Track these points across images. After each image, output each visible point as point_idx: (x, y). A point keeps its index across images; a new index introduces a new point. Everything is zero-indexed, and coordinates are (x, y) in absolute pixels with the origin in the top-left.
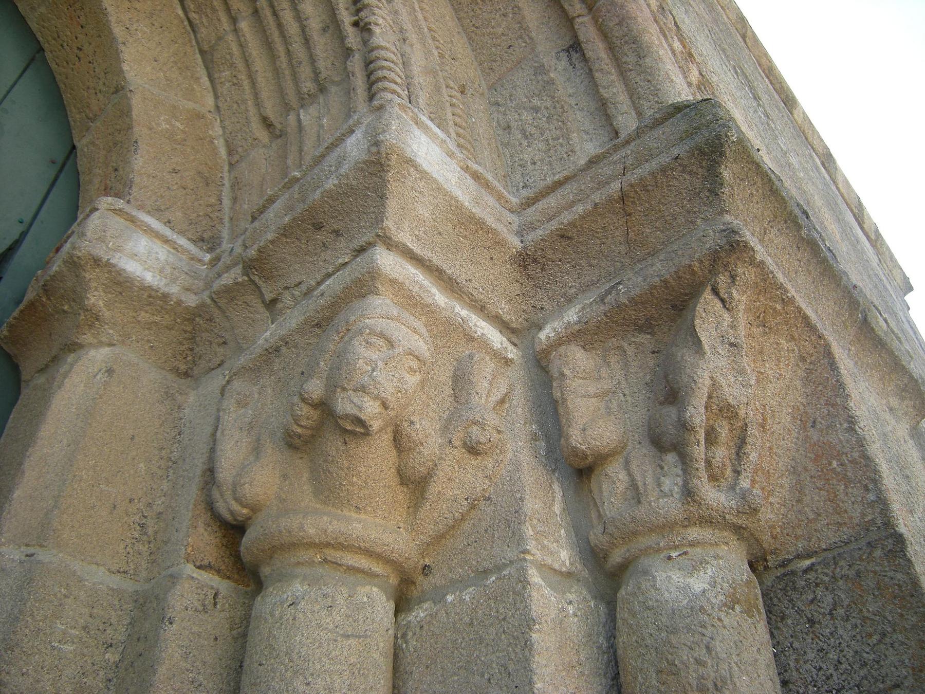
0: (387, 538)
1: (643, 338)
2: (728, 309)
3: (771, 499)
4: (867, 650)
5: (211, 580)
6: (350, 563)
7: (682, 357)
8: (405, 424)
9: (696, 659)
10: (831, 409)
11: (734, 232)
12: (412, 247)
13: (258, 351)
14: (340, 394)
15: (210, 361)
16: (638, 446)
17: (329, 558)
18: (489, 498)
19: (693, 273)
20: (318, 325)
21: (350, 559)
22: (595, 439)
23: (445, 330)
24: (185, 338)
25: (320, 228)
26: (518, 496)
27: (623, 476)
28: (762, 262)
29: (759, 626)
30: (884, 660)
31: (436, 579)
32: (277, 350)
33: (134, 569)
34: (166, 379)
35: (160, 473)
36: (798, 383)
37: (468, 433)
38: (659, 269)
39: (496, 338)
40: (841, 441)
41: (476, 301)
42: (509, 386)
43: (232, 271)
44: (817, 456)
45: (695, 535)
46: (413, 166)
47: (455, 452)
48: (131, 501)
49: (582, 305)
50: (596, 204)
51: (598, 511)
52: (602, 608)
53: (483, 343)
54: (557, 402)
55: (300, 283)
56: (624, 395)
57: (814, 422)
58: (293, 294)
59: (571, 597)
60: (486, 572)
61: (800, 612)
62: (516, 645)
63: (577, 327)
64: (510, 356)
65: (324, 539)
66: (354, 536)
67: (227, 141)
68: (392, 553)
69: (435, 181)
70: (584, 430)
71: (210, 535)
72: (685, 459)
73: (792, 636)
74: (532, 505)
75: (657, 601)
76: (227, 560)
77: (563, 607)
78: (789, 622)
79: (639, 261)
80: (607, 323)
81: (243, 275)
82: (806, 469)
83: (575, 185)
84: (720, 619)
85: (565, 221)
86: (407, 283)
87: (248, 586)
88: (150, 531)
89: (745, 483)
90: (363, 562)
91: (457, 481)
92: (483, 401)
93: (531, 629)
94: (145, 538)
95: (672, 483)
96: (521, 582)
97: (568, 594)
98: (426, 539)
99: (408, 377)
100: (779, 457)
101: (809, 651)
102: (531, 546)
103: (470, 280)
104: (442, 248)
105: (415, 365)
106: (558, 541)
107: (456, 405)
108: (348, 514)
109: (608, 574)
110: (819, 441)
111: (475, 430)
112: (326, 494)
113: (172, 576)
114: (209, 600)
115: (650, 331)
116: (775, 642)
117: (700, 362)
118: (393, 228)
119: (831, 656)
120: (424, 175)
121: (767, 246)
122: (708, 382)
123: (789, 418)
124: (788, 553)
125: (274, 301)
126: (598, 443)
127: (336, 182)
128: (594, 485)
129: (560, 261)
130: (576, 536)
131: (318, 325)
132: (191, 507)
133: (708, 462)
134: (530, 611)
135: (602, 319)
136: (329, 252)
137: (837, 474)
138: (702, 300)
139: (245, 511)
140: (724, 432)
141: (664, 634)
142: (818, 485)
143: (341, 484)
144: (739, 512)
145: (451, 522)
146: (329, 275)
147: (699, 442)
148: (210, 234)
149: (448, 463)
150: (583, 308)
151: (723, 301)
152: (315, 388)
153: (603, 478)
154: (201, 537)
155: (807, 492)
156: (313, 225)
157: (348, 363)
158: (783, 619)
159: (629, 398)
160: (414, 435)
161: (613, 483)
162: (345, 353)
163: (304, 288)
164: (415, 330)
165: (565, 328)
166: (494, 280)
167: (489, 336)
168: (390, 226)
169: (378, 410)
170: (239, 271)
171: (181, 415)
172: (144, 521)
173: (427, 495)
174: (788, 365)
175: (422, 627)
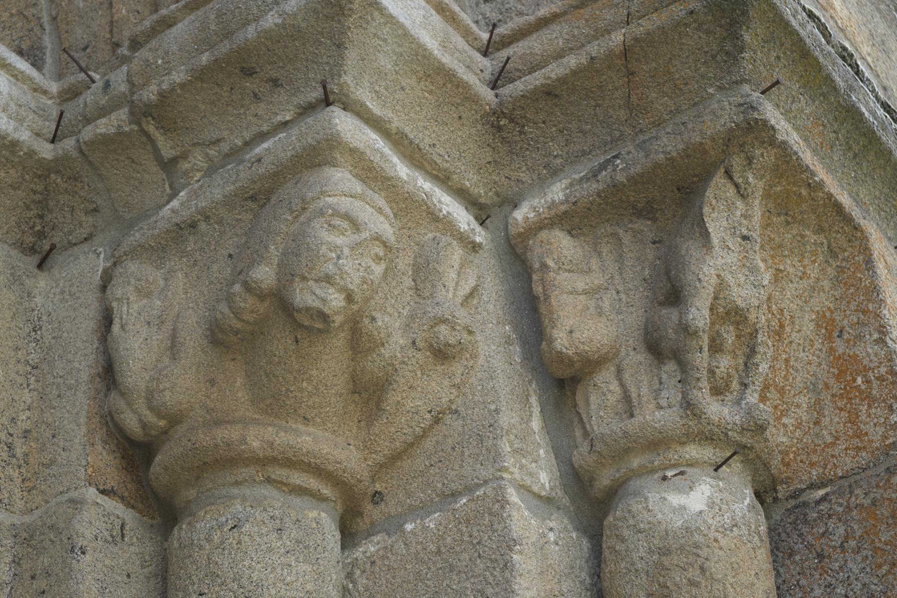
0: (339, 454)
1: (643, 225)
2: (742, 196)
3: (785, 420)
4: (875, 581)
5: (115, 508)
6: (298, 482)
7: (687, 250)
8: (366, 321)
9: (689, 580)
10: (862, 317)
11: (752, 107)
12: (371, 107)
13: (163, 225)
14: (298, 285)
15: (70, 233)
16: (632, 353)
17: (273, 477)
18: (456, 411)
19: (705, 152)
20: (253, 198)
22: (583, 343)
23: (406, 206)
25: (251, 75)
26: (493, 407)
27: (615, 386)
28: (784, 143)
29: (759, 552)
30: (891, 591)
31: (390, 507)
32: (193, 225)
33: (8, 498)
34: (10, 257)
35: (20, 380)
36: (826, 284)
37: (435, 333)
38: (667, 144)
39: (464, 219)
40: (868, 354)
41: (439, 170)
42: (479, 277)
43: (114, 116)
44: (841, 372)
45: (694, 454)
46: (378, 9)
47: (419, 355)
49: (569, 181)
50: (592, 58)
51: (584, 428)
52: (585, 543)
53: (447, 224)
54: (538, 298)
55: (219, 140)
56: (618, 293)
57: (841, 331)
58: (207, 154)
59: (552, 524)
60: (455, 495)
61: (809, 547)
62: (494, 568)
63: (563, 208)
64: (478, 239)
65: (269, 452)
66: (304, 450)
68: (344, 472)
69: (401, 26)
70: (571, 332)
71: (108, 454)
72: (684, 366)
73: (799, 574)
74: (508, 418)
75: (649, 523)
76: (129, 486)
77: (543, 533)
78: (797, 558)
79: (641, 131)
80: (600, 204)
81: (131, 123)
82: (827, 386)
83: (566, 28)
84: (716, 540)
85: (553, 76)
86: (368, 152)
87: (153, 518)
88: (19, 452)
89: (752, 398)
90: (313, 483)
91: (419, 389)
92: (451, 295)
93: (511, 550)
94: (14, 461)
95: (672, 394)
96: (498, 501)
97: (548, 521)
98: (379, 458)
100: (797, 371)
101: (816, 587)
102: (509, 462)
103: (434, 145)
106: (536, 462)
107: (417, 300)
108: (294, 426)
109: (593, 503)
110: (844, 354)
111: (443, 329)
112: (269, 402)
113: (72, 501)
114: (116, 531)
115: (651, 215)
116: (780, 581)
117: (707, 257)
118: (352, 84)
119: (839, 591)
120: (390, 19)
121: (795, 117)
122: (714, 280)
123: (812, 326)
124: (801, 482)
125: (174, 160)
126: (586, 348)
127: (279, 21)
128: (579, 397)
129: (544, 122)
130: (556, 458)
131: (253, 198)
132: (83, 420)
133: (711, 372)
134: (510, 531)
135: (594, 200)
136: (262, 105)
137: (861, 392)
138: (713, 184)
139: (162, 423)
140: (729, 337)
141: (655, 557)
142: (839, 404)
143: (287, 390)
144: (743, 429)
145: (410, 439)
146: (262, 136)
147: (701, 348)
148: (28, 43)
149: (410, 368)
150: (571, 185)
151: (737, 186)
152: (265, 274)
153: (591, 388)
154: (100, 457)
155: (827, 413)
156: (243, 70)
157: (309, 249)
158: (791, 555)
159: (623, 296)
160: (375, 333)
161: (601, 401)
162: (304, 237)
163: (225, 147)
164: (380, 211)
165: (549, 208)
166: (456, 142)
167: (455, 215)
168: (349, 82)
169: (343, 304)
170: (124, 117)
171: (33, 305)
172: (10, 440)
173: (383, 406)
174: (814, 262)
175: (373, 563)
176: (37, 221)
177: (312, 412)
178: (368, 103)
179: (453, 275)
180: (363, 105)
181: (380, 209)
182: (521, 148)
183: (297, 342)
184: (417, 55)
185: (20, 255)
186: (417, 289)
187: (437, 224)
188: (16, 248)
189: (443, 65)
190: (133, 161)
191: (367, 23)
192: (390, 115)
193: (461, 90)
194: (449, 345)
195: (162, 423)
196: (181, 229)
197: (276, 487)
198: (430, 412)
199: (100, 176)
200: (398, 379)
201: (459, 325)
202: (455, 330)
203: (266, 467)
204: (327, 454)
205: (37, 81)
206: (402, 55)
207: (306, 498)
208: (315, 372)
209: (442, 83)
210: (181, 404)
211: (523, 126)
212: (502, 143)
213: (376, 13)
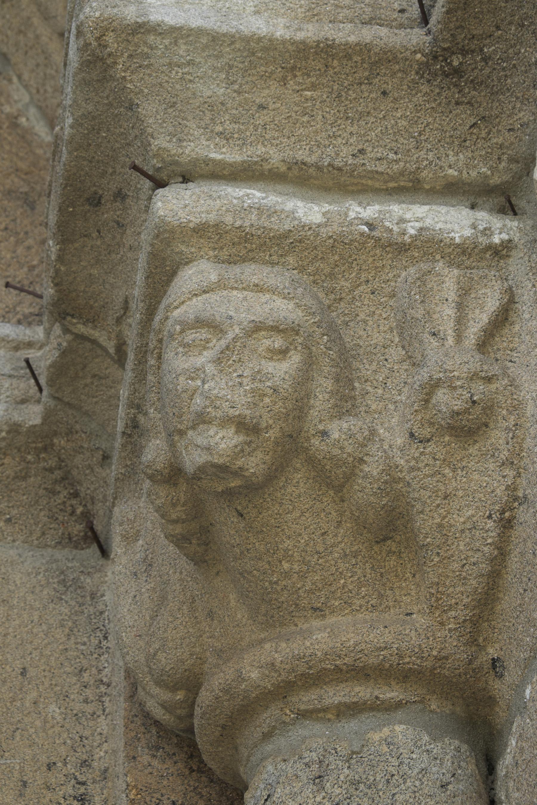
6: (337, 700)
12: (219, 157)
17: (302, 707)
21: (335, 695)
24: (56, 482)
25: (99, 202)
39: (456, 222)
41: (392, 179)
46: (149, 31)
47: (431, 447)
48: (49, 767)
53: (428, 246)
66: (319, 654)
67: (40, 108)
68: (401, 657)
69: (200, 32)
90: (362, 692)
98: (461, 613)
99: (269, 367)
103: (362, 151)
104: (279, 128)
105: (278, 343)
111: (441, 396)
120: (177, 33)
129: (498, 28)
139: (180, 696)
143: (270, 582)
145: (485, 567)
149: (427, 471)
160: (336, 451)
164: (258, 288)
168: (165, 145)
171: (101, 607)
172: (82, 790)
176: (74, 502)
177: (319, 597)
178: (213, 155)
179: (449, 311)
180: (207, 161)
181: (257, 285)
182: (499, 80)
183: (242, 516)
184: (253, 54)
185: (74, 552)
186: (410, 357)
187: (409, 253)
188: (64, 547)
189: (303, 42)
190: (101, 378)
191: (147, 56)
192: (261, 150)
193: (356, 58)
194: (458, 414)
195: (180, 696)
196: (130, 436)
197: (318, 719)
198: (490, 517)
199: (86, 413)
200: (416, 495)
201: (458, 378)
202: (455, 388)
203: (289, 698)
204: (356, 645)
205: (13, 335)
206: (231, 67)
207: (363, 717)
208: (288, 543)
209: (320, 66)
210: (183, 662)
211: (481, 50)
212: (475, 89)
213: (151, 38)
